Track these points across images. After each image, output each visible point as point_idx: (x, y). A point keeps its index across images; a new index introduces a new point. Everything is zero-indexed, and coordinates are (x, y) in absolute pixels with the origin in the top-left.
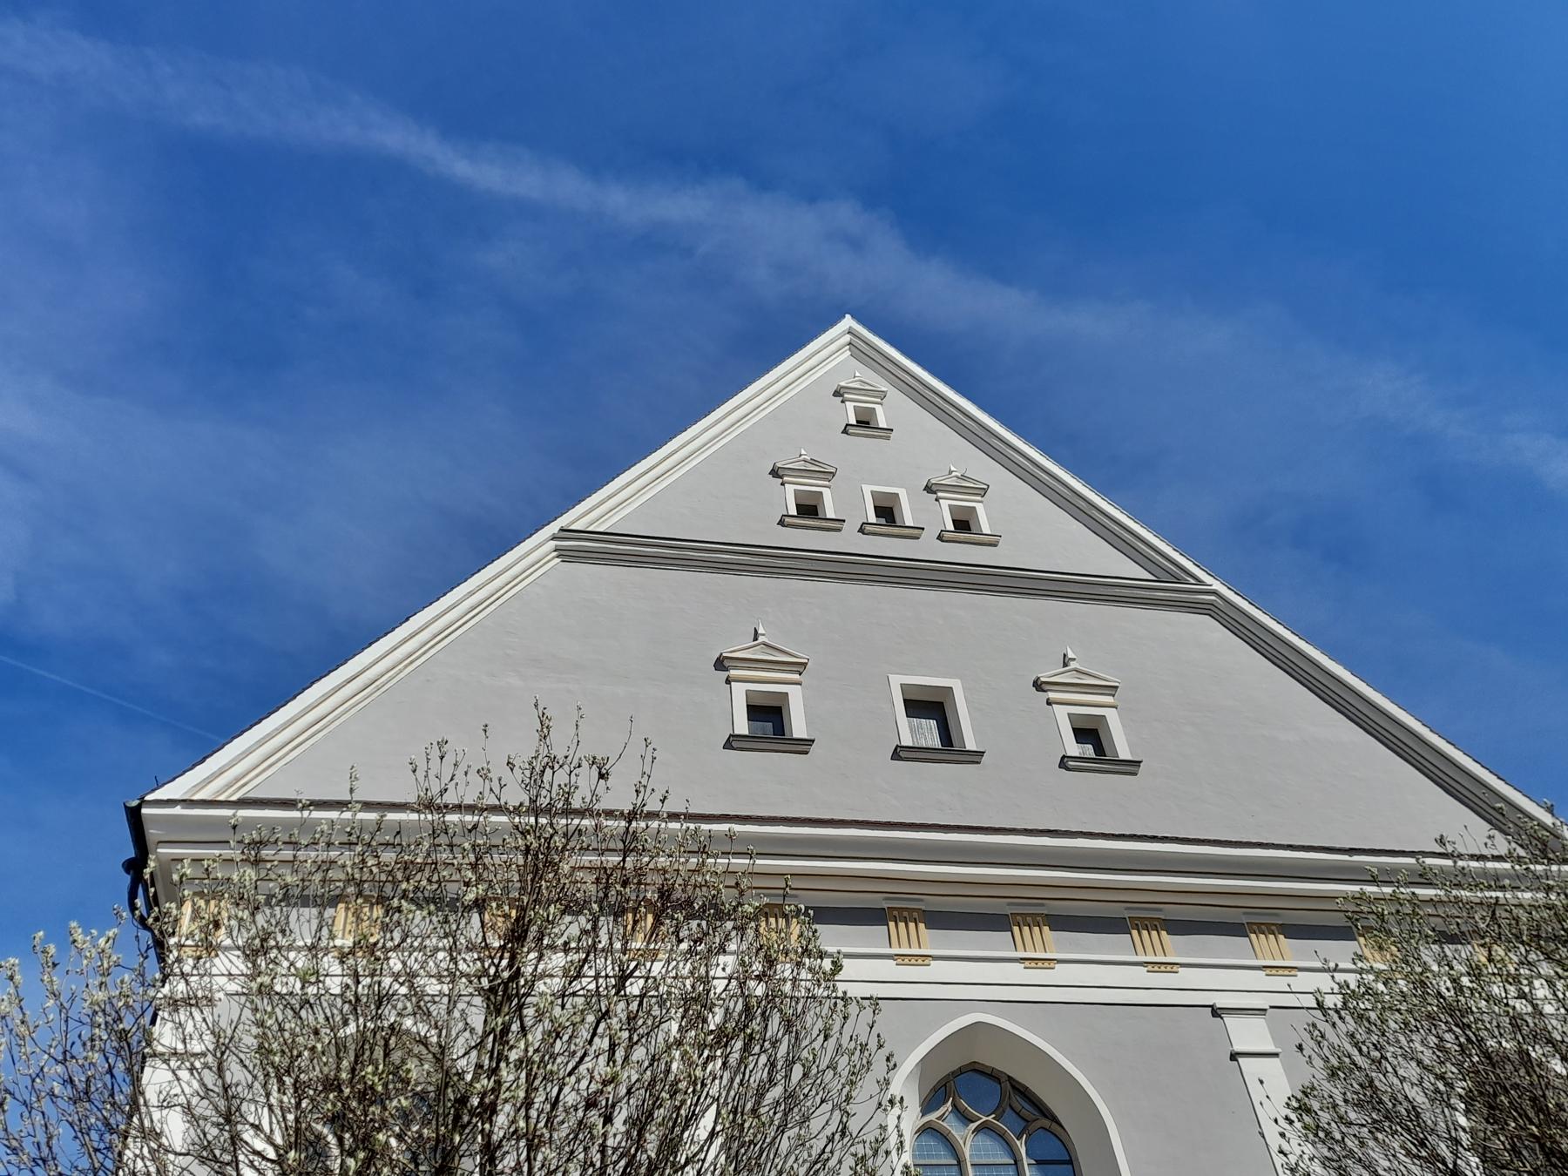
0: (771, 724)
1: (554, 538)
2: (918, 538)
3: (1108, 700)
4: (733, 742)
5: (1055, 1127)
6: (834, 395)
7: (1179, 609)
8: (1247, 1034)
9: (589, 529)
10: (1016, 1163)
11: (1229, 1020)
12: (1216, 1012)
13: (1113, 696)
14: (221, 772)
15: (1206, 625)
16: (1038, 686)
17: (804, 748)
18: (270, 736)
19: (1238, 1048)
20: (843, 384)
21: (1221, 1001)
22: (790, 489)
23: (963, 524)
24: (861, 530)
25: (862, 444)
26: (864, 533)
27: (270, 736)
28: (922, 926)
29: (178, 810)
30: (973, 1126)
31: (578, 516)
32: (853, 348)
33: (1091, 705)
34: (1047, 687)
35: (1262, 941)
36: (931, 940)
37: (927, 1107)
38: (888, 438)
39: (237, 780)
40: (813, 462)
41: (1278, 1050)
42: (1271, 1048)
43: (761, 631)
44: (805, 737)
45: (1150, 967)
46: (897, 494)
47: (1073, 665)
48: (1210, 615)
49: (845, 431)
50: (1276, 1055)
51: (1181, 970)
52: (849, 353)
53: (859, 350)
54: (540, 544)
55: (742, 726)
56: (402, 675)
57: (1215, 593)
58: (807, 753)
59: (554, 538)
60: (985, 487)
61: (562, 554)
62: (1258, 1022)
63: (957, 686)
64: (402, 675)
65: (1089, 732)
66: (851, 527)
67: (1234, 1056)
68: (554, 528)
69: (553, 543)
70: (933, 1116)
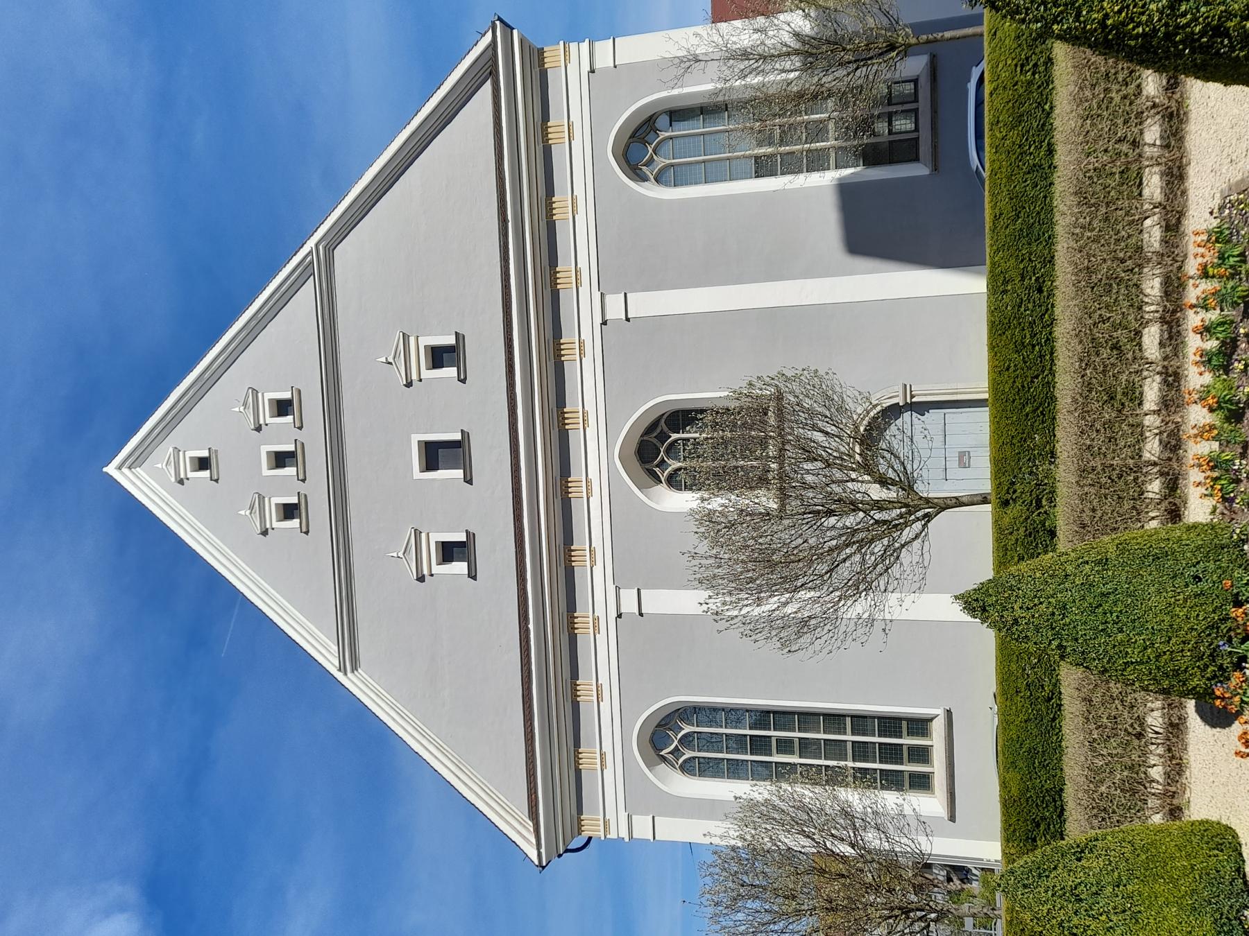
0: (444, 355)
1: (345, 674)
2: (303, 444)
4: (468, 480)
5: (654, 118)
6: (183, 484)
7: (333, 276)
8: (615, 310)
9: (337, 655)
10: (671, 138)
11: (608, 317)
12: (604, 323)
13: (421, 532)
14: (519, 832)
15: (342, 253)
16: (409, 384)
17: (471, 536)
18: (497, 813)
19: (612, 65)
20: (173, 479)
21: (598, 320)
23: (283, 408)
24: (304, 481)
25: (223, 464)
26: (305, 479)
27: (497, 813)
28: (569, 479)
29: (543, 850)
30: (655, 157)
31: (330, 662)
32: (133, 466)
34: (409, 380)
36: (577, 474)
37: (644, 179)
38: (216, 451)
39: (521, 823)
40: (252, 508)
42: (623, 295)
44: (454, 336)
45: (582, 356)
47: (391, 360)
48: (333, 250)
49: (217, 481)
51: (600, 682)
52: (138, 469)
53: (136, 460)
54: (352, 682)
55: (451, 372)
56: (450, 750)
57: (317, 245)
58: (474, 534)
59: (345, 674)
60: (250, 390)
61: (354, 668)
63: (417, 474)
64: (450, 750)
67: (615, 67)
68: (339, 676)
69: (349, 675)
70: (663, 480)
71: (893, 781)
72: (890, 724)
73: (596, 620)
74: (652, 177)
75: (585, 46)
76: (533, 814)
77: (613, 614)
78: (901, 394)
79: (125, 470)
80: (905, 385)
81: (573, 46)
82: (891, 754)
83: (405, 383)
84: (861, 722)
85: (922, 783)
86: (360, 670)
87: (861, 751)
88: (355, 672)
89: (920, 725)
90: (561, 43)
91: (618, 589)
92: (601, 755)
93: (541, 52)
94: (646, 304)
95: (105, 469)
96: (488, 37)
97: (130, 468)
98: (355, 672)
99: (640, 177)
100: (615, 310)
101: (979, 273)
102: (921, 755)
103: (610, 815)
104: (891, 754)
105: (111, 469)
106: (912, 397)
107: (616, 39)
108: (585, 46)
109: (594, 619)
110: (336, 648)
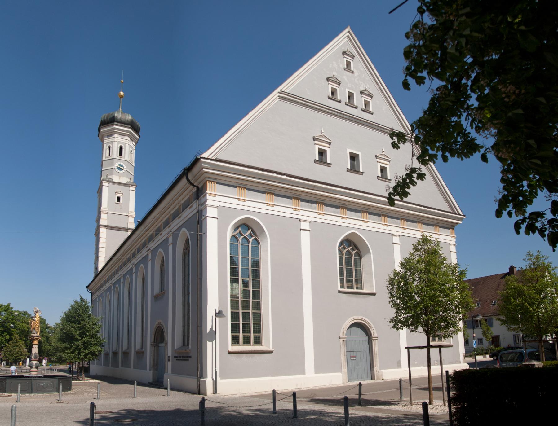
3: (388, 163)
8: (396, 240)
12: (392, 235)
16: (376, 157)
19: (394, 242)
21: (394, 233)
22: (364, 99)
33: (385, 164)
35: (417, 225)
41: (218, 217)
42: (399, 243)
43: (323, 131)
45: (267, 204)
46: (353, 93)
47: (384, 153)
50: (399, 244)
59: (279, 93)
61: (280, 97)
62: (398, 238)
65: (383, 170)
66: (343, 103)
67: (393, 243)
68: (278, 90)
71: (235, 328)
72: (258, 329)
73: (298, 210)
74: (235, 234)
75: (454, 243)
76: (216, 160)
77: (301, 218)
78: (375, 336)
79: (348, 34)
80: (377, 338)
81: (455, 240)
82: (246, 328)
83: (377, 156)
84: (258, 317)
85: (235, 340)
86: (279, 99)
87: (246, 316)
88: (278, 97)
89: (258, 341)
90: (456, 236)
91: (217, 207)
92: (245, 200)
93: (453, 229)
94: (305, 237)
95: (349, 27)
96: (461, 214)
97: (348, 36)
98: (278, 97)
99: (236, 227)
100: (396, 240)
102: (247, 341)
103: (218, 198)
104: (246, 328)
105: (348, 29)
106: (374, 340)
107: (309, 232)
108: (135, 190)
109: (298, 209)
110: (287, 92)
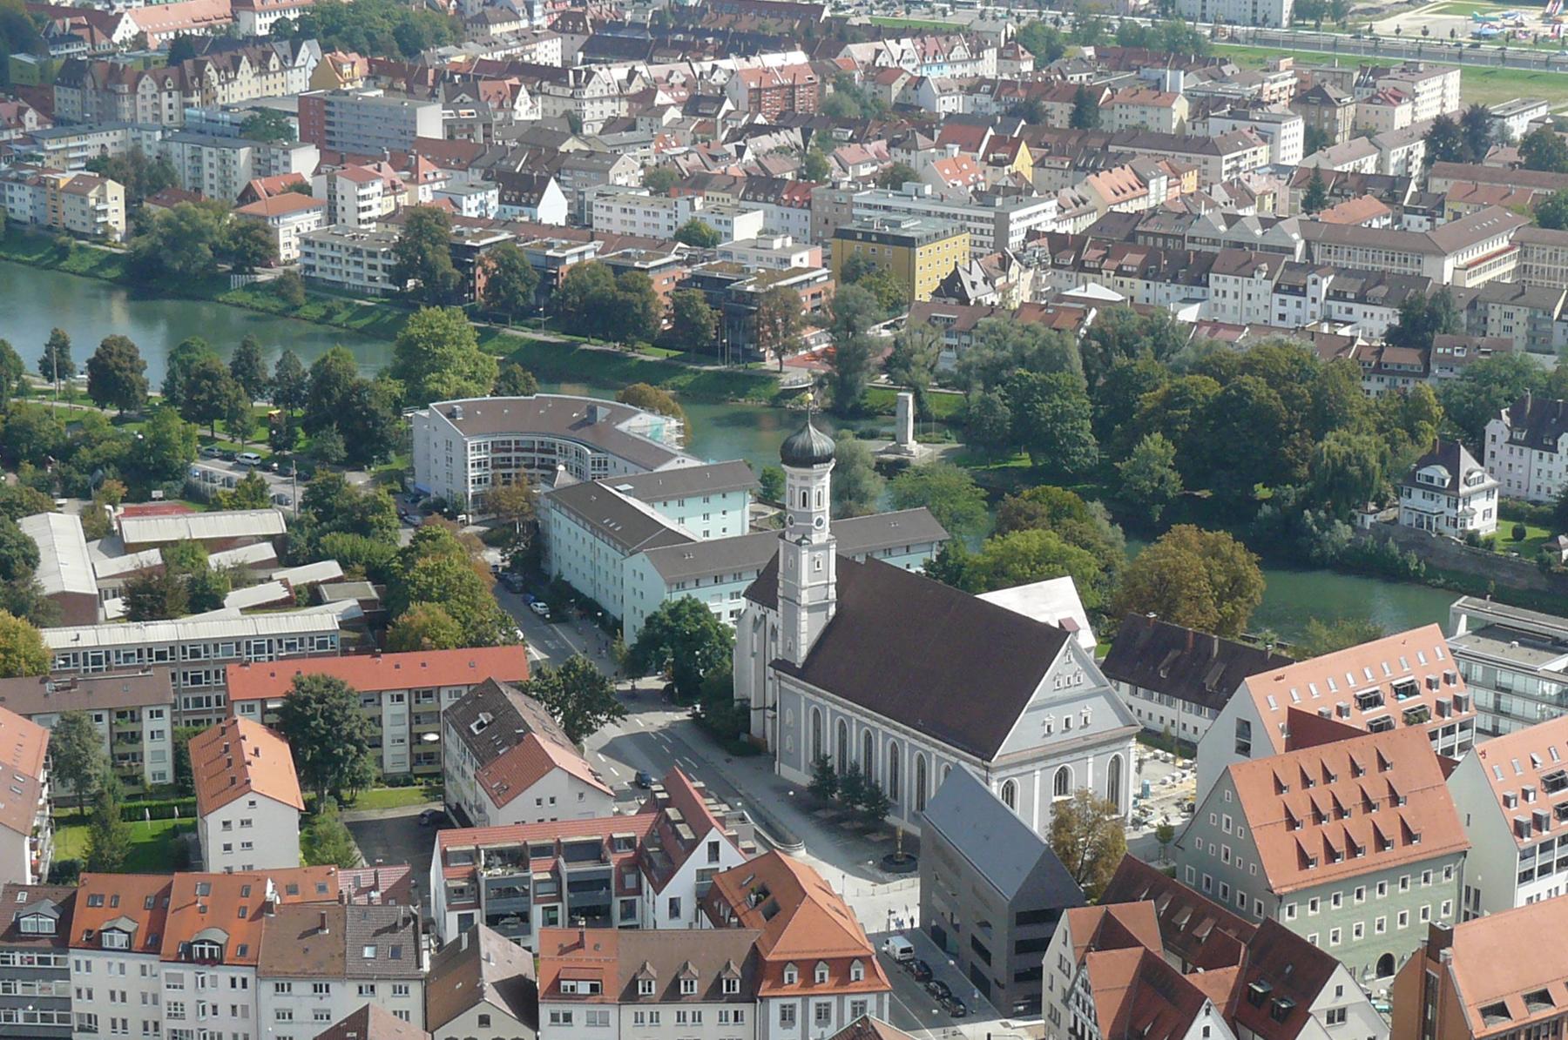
25: (557, 801)
101: (906, 882)
